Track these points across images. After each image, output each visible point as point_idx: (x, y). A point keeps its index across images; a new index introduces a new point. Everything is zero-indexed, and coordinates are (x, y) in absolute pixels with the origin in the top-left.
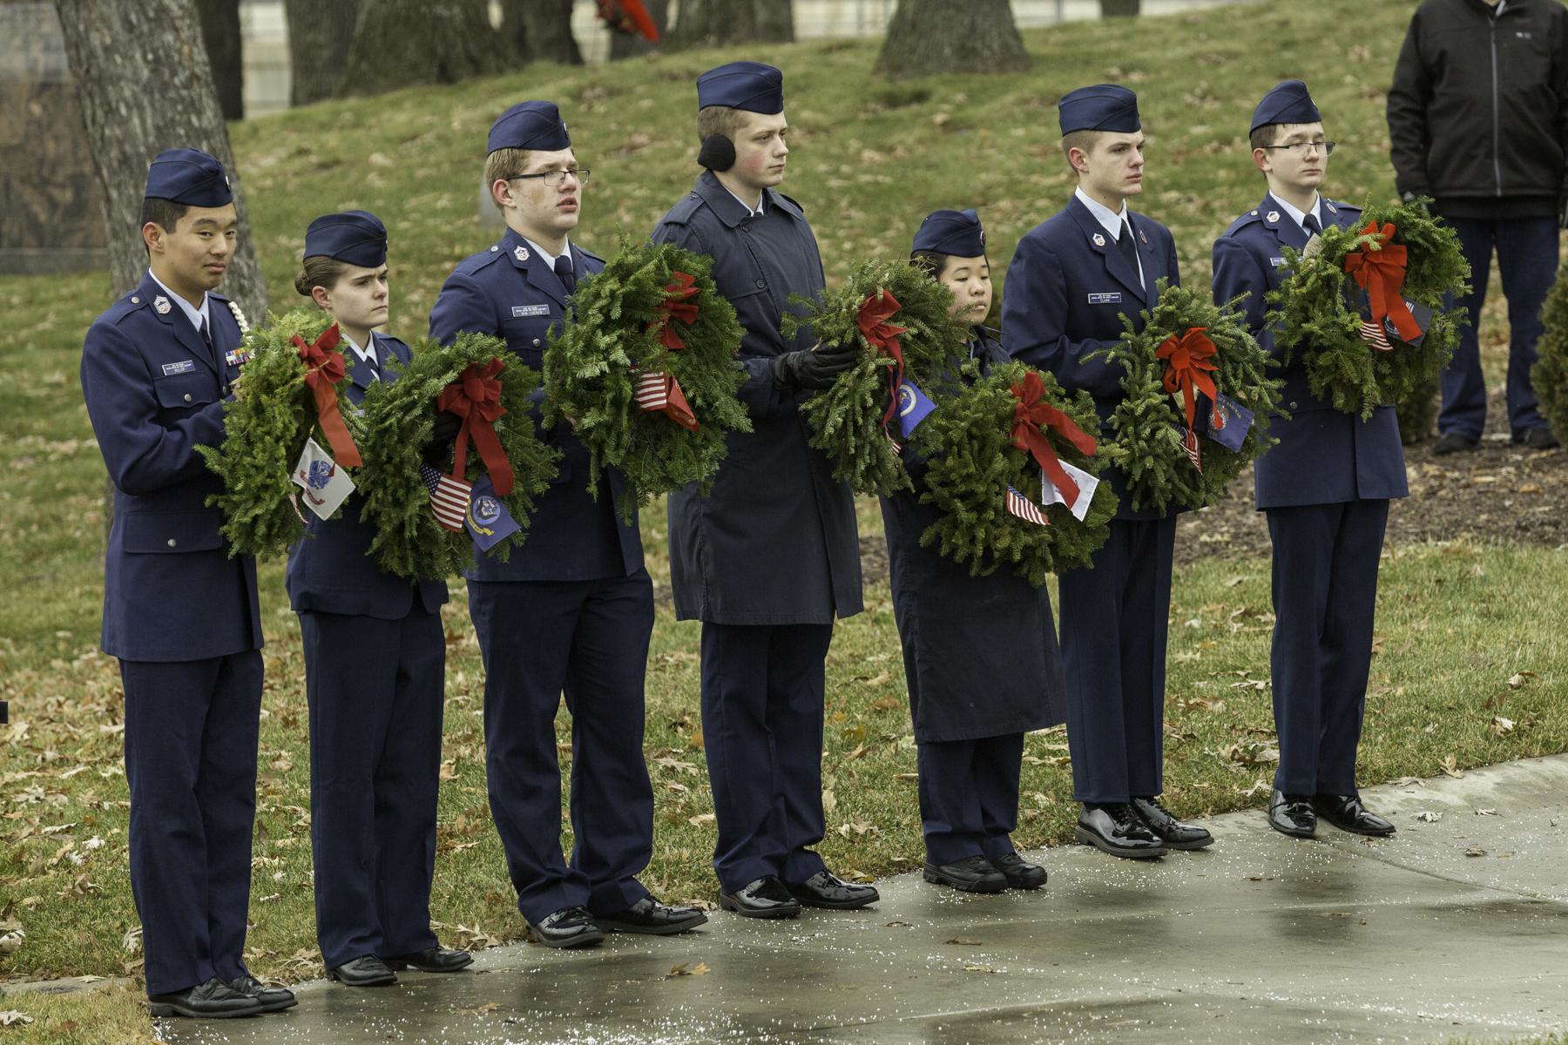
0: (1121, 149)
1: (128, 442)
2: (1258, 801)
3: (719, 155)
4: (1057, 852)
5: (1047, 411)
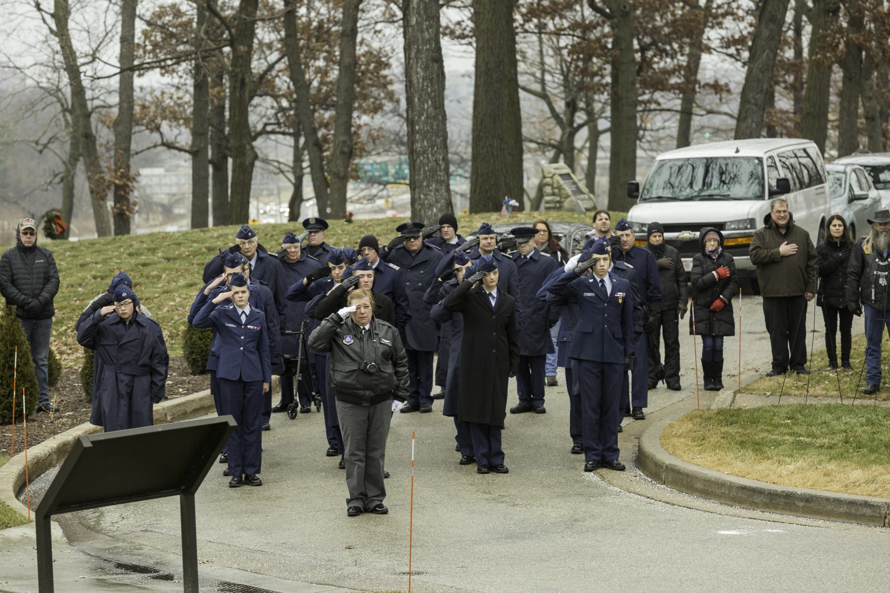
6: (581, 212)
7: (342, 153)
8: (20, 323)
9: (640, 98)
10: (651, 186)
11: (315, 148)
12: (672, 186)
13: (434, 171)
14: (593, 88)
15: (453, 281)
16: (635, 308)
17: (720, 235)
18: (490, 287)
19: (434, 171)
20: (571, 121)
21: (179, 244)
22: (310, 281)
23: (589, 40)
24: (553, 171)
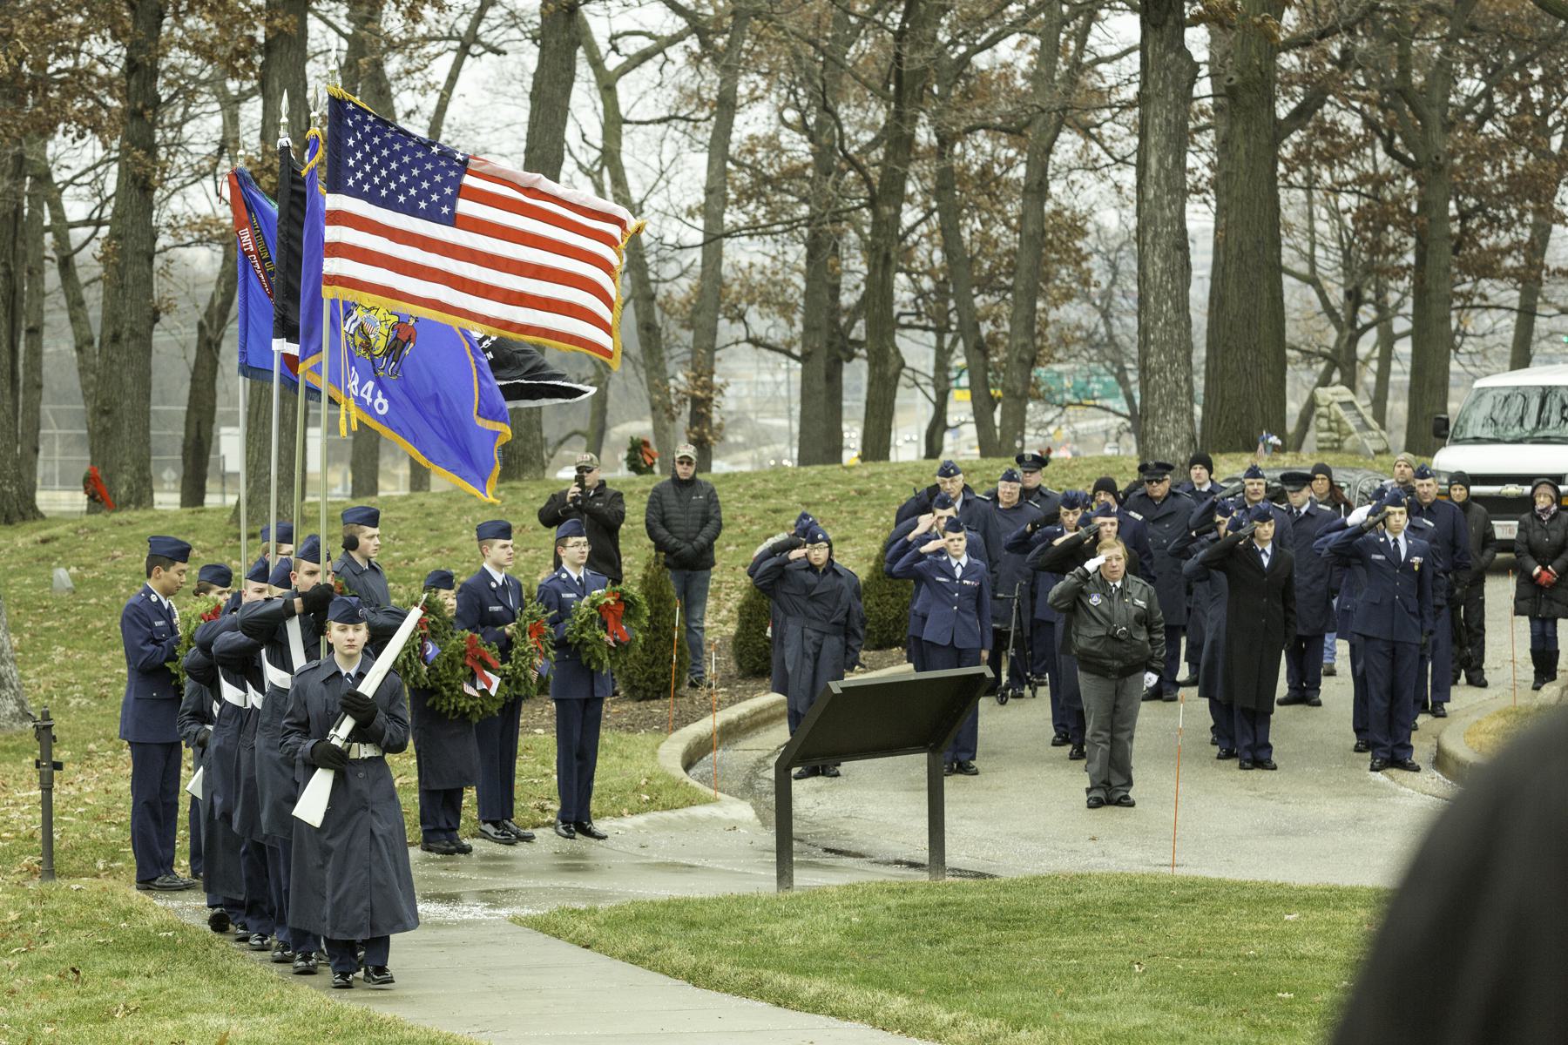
0: (505, 546)
1: (144, 652)
2: (549, 824)
3: (351, 544)
4: (480, 841)
5: (479, 651)
6: (1368, 456)
7: (1021, 360)
8: (669, 573)
9: (1458, 289)
10: (1466, 421)
11: (977, 352)
12: (1495, 422)
13: (1173, 396)
14: (1387, 272)
15: (1212, 535)
16: (1435, 576)
17: (1557, 491)
18: (1262, 541)
19: (1173, 396)
20: (1353, 320)
21: (819, 485)
22: (1034, 528)
23: (1382, 201)
24: (1331, 398)
